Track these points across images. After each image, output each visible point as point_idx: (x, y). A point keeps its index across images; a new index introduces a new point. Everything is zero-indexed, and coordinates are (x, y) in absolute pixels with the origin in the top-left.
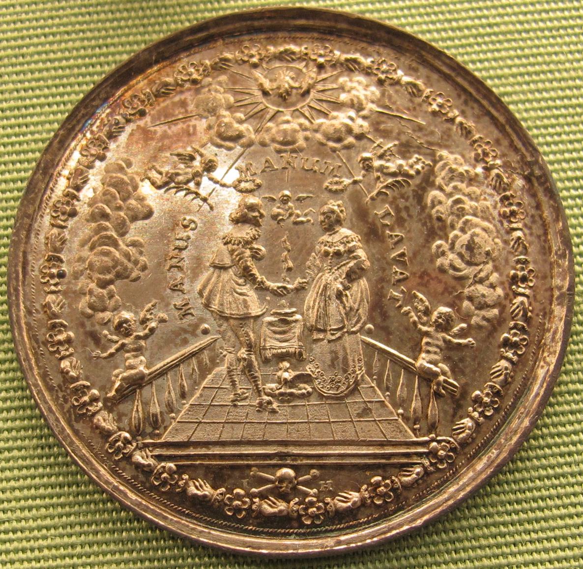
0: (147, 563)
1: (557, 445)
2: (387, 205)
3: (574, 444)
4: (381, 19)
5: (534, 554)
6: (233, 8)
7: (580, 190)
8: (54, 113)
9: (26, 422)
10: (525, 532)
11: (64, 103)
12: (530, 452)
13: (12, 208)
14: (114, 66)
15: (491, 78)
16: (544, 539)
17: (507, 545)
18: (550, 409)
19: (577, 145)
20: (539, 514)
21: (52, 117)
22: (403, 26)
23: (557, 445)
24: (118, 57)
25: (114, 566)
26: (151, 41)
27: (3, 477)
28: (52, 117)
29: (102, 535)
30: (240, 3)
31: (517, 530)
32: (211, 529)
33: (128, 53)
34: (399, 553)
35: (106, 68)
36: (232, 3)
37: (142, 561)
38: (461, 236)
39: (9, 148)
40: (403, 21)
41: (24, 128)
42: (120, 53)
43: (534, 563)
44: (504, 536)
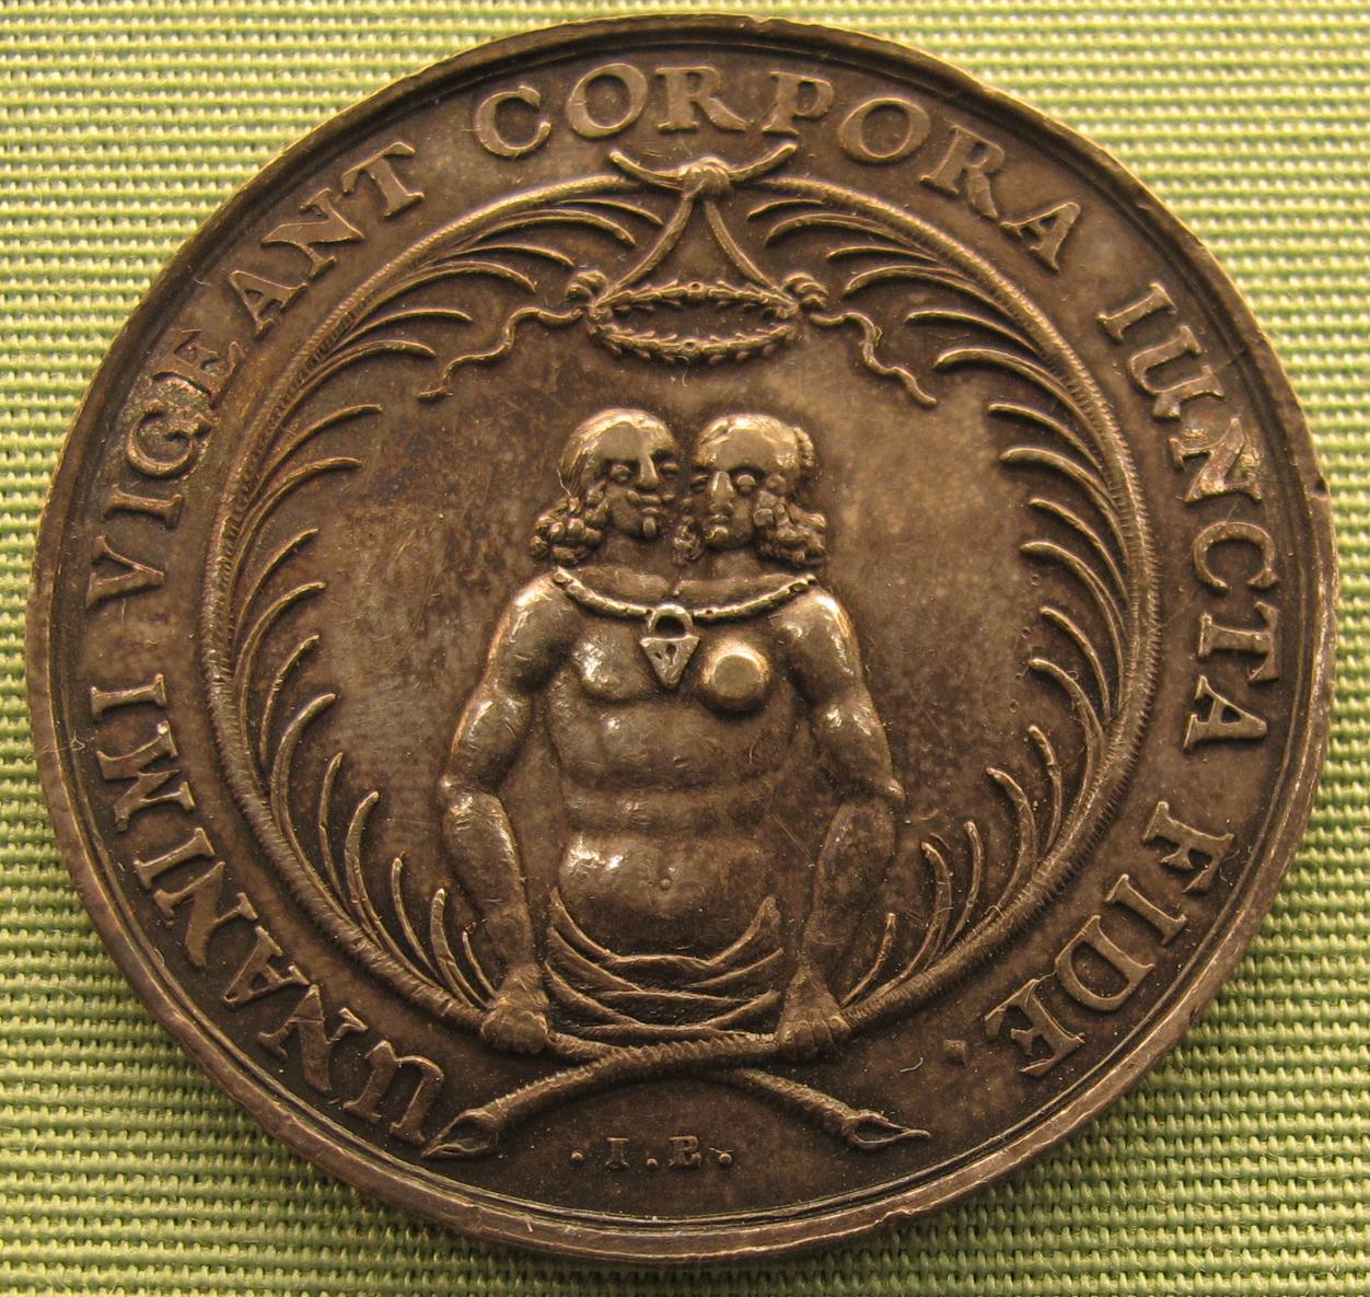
1: (1291, 1112)
4: (874, 31)
5: (1321, 1207)
6: (539, 17)
8: (195, 200)
11: (218, 181)
14: (333, 114)
15: (1197, 216)
16: (1253, 1223)
17: (1279, 1089)
21: (187, 207)
22: (937, 50)
23: (1291, 1112)
24: (238, 170)
26: (407, 69)
27: (7, 606)
28: (187, 207)
30: (557, 7)
31: (1231, 1106)
33: (392, 71)
35: (316, 114)
36: (539, 7)
38: (649, 613)
39: (18, 302)
40: (937, 40)
41: (143, 224)
42: (245, 163)
43: (76, 1287)
44: (1292, 982)
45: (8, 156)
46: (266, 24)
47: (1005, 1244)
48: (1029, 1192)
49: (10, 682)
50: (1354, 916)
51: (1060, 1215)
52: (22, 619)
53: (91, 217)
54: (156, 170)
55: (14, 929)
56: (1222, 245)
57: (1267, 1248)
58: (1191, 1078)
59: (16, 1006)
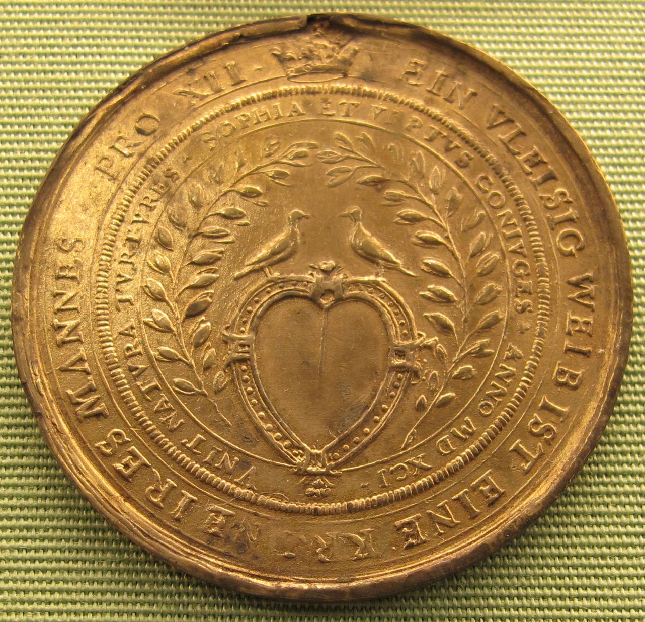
0: (116, 617)
2: (535, 414)
3: (635, 424)
7: (641, 611)
9: (41, 460)
10: (573, 588)
12: (577, 488)
13: (17, 224)
18: (600, 448)
19: (639, 224)
20: (563, 551)
25: (159, 617)
29: (133, 585)
32: (315, 582)
34: (391, 613)
37: (137, 614)
45: (5, 129)
46: (70, 67)
47: (445, 604)
48: (464, 581)
49: (4, 313)
50: (625, 436)
51: (479, 591)
52: (10, 282)
53: (20, 54)
54: (38, 84)
55: (6, 416)
56: (564, 107)
57: (581, 587)
58: (554, 529)
59: (7, 472)
